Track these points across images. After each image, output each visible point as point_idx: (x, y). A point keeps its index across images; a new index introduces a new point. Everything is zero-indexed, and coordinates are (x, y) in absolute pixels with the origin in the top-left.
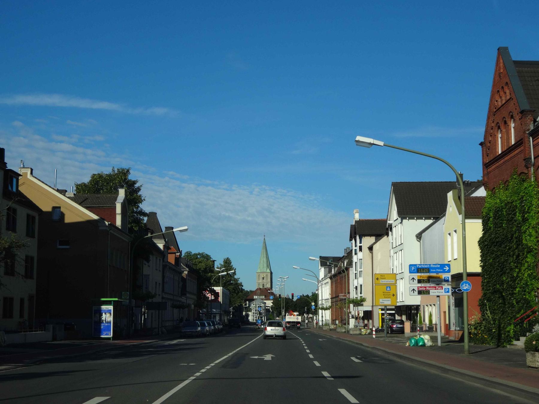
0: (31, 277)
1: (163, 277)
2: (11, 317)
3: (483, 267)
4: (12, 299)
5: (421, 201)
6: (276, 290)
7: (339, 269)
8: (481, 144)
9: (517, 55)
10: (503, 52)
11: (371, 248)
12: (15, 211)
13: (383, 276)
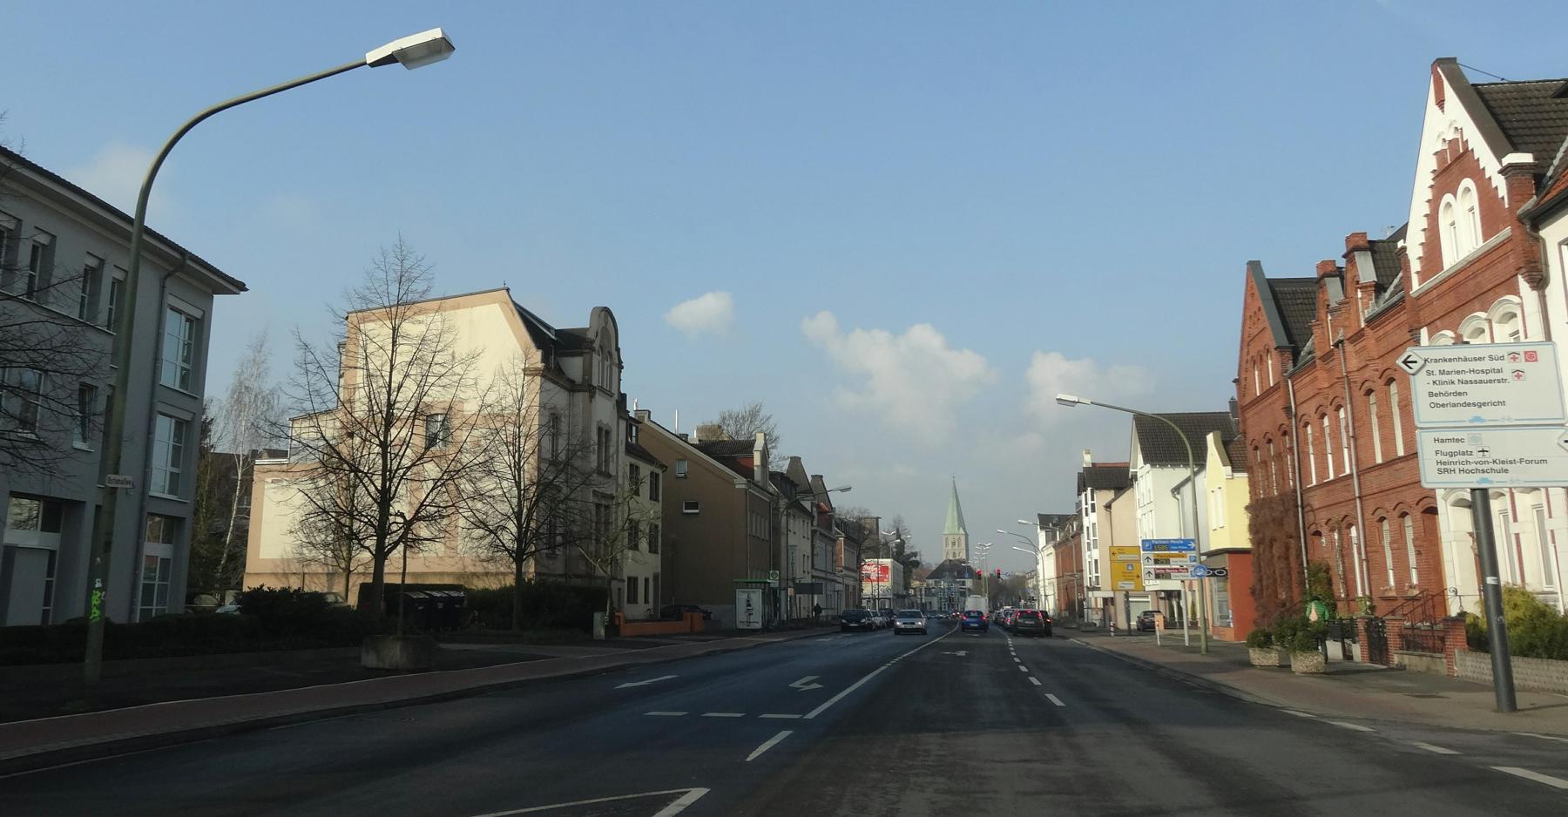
1: (813, 547)
3: (1255, 528)
5: (1171, 440)
6: (974, 563)
7: (1063, 530)
8: (1235, 381)
9: (1270, 273)
10: (1254, 267)
11: (1108, 507)
13: (1122, 550)
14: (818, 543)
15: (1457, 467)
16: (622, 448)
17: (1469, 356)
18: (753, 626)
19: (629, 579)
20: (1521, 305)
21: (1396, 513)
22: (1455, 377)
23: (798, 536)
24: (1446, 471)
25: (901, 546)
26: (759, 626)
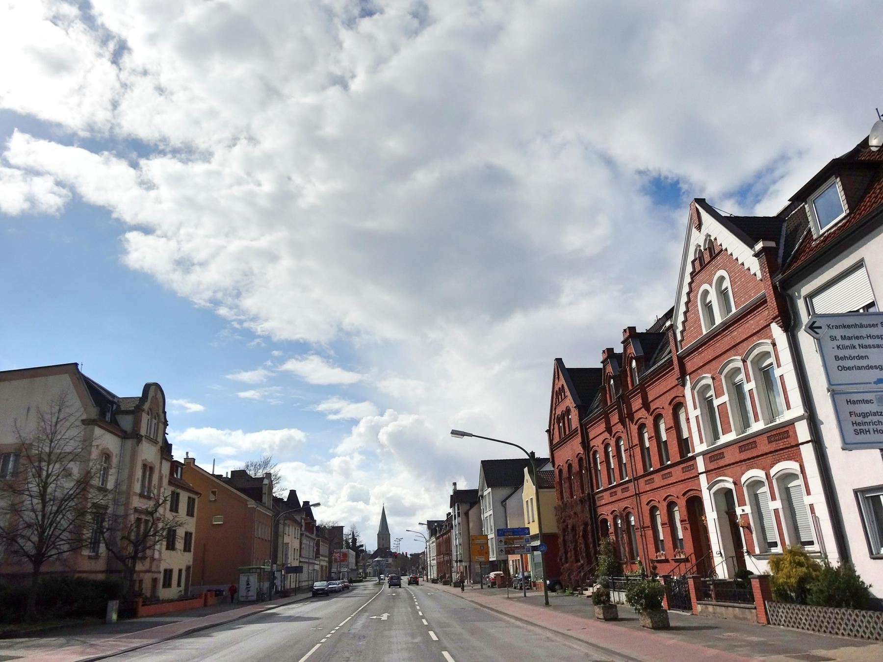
0: (189, 551)
1: (301, 544)
2: (169, 586)
4: (171, 571)
9: (568, 365)
10: (559, 361)
12: (178, 494)
14: (304, 541)
15: (871, 427)
16: (165, 481)
17: (864, 323)
18: (250, 599)
19: (165, 571)
20: (774, 345)
21: (665, 504)
22: (855, 342)
23: (291, 538)
24: (861, 432)
25: (354, 540)
26: (255, 598)
